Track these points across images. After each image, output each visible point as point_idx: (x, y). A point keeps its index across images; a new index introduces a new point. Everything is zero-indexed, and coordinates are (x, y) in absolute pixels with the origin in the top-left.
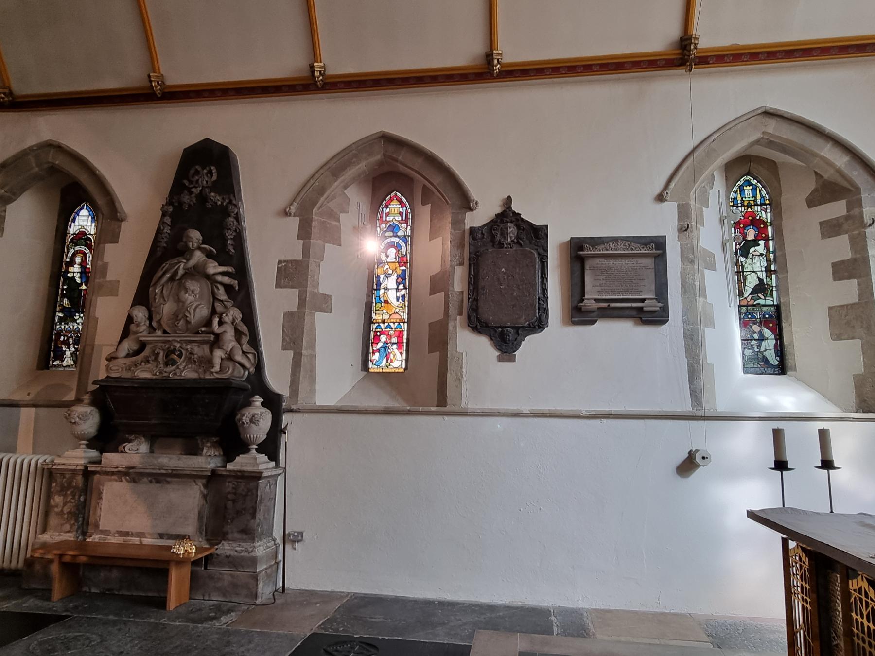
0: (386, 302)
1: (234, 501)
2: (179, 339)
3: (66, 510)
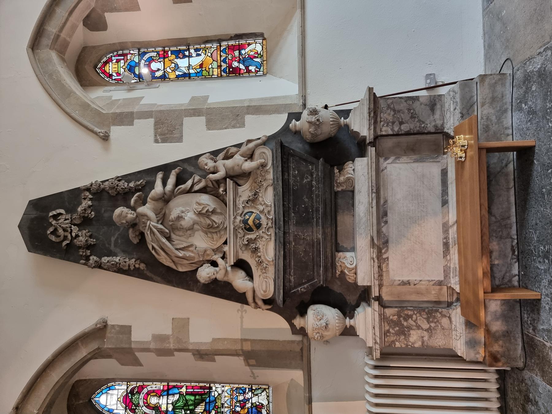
0: (201, 66)
1: (401, 123)
2: (232, 217)
3: (425, 326)
